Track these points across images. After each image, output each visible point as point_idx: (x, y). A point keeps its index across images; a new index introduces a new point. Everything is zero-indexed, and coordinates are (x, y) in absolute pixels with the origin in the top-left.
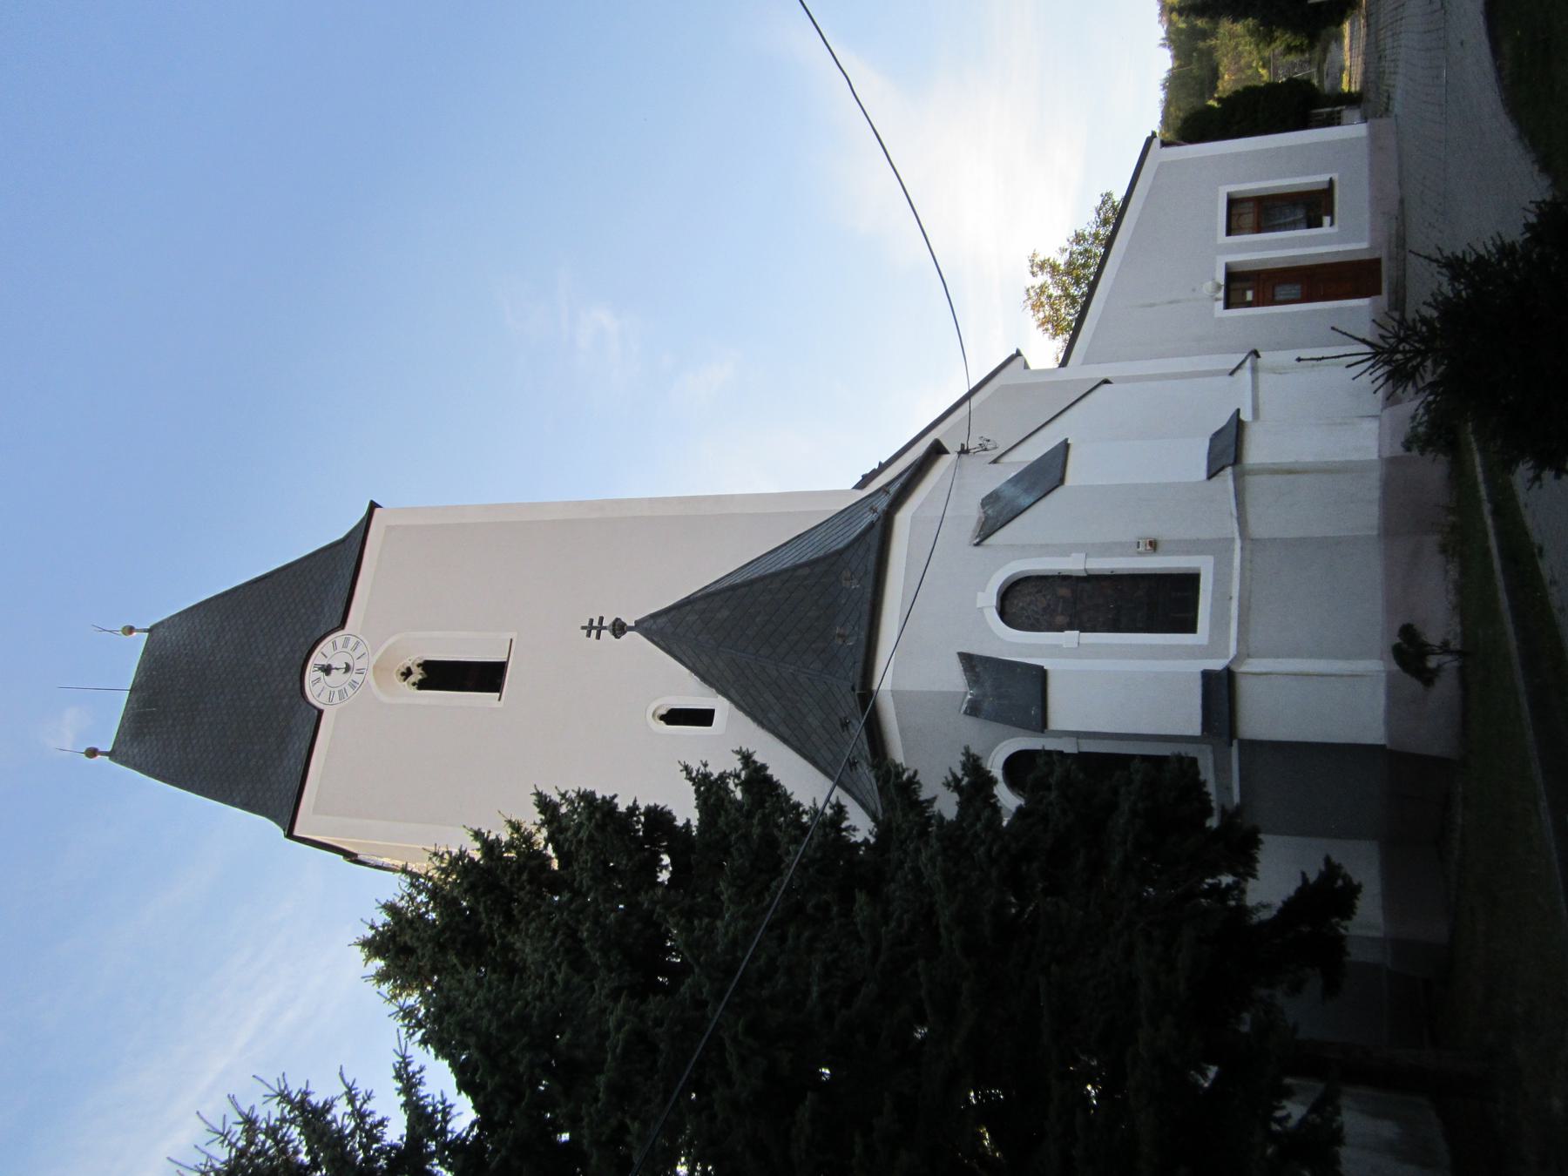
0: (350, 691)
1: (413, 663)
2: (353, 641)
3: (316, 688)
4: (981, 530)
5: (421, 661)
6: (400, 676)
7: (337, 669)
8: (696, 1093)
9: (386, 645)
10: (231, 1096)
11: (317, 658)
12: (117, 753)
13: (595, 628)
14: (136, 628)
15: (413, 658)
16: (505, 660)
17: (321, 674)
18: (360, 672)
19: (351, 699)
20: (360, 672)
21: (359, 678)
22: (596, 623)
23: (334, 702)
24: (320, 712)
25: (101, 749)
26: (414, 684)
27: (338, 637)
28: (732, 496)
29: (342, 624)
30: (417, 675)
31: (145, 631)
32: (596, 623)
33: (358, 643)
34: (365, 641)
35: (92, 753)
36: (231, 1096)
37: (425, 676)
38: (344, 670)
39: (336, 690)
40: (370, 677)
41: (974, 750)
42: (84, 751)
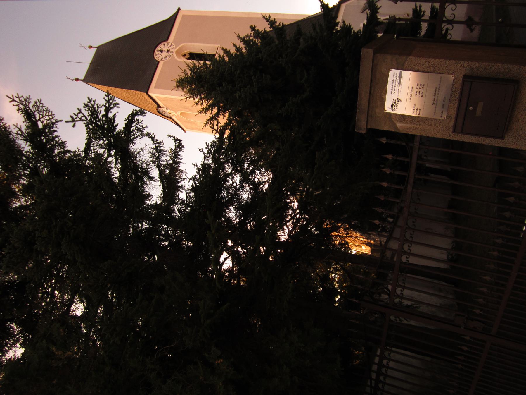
0: (168, 57)
1: (187, 53)
2: (170, 44)
3: (157, 56)
4: (364, 8)
5: (189, 52)
7: (165, 51)
8: (243, 217)
9: (180, 46)
11: (159, 48)
13: (249, 36)
14: (93, 46)
15: (187, 51)
16: (215, 54)
18: (172, 52)
20: (172, 52)
21: (171, 54)
22: (249, 35)
23: (163, 60)
24: (159, 62)
25: (80, 79)
26: (186, 58)
27: (166, 43)
28: (288, 14)
29: (167, 40)
30: (188, 56)
31: (96, 47)
32: (249, 35)
34: (174, 45)
35: (77, 80)
36: (154, 134)
39: (164, 57)
40: (175, 54)
41: (379, 13)
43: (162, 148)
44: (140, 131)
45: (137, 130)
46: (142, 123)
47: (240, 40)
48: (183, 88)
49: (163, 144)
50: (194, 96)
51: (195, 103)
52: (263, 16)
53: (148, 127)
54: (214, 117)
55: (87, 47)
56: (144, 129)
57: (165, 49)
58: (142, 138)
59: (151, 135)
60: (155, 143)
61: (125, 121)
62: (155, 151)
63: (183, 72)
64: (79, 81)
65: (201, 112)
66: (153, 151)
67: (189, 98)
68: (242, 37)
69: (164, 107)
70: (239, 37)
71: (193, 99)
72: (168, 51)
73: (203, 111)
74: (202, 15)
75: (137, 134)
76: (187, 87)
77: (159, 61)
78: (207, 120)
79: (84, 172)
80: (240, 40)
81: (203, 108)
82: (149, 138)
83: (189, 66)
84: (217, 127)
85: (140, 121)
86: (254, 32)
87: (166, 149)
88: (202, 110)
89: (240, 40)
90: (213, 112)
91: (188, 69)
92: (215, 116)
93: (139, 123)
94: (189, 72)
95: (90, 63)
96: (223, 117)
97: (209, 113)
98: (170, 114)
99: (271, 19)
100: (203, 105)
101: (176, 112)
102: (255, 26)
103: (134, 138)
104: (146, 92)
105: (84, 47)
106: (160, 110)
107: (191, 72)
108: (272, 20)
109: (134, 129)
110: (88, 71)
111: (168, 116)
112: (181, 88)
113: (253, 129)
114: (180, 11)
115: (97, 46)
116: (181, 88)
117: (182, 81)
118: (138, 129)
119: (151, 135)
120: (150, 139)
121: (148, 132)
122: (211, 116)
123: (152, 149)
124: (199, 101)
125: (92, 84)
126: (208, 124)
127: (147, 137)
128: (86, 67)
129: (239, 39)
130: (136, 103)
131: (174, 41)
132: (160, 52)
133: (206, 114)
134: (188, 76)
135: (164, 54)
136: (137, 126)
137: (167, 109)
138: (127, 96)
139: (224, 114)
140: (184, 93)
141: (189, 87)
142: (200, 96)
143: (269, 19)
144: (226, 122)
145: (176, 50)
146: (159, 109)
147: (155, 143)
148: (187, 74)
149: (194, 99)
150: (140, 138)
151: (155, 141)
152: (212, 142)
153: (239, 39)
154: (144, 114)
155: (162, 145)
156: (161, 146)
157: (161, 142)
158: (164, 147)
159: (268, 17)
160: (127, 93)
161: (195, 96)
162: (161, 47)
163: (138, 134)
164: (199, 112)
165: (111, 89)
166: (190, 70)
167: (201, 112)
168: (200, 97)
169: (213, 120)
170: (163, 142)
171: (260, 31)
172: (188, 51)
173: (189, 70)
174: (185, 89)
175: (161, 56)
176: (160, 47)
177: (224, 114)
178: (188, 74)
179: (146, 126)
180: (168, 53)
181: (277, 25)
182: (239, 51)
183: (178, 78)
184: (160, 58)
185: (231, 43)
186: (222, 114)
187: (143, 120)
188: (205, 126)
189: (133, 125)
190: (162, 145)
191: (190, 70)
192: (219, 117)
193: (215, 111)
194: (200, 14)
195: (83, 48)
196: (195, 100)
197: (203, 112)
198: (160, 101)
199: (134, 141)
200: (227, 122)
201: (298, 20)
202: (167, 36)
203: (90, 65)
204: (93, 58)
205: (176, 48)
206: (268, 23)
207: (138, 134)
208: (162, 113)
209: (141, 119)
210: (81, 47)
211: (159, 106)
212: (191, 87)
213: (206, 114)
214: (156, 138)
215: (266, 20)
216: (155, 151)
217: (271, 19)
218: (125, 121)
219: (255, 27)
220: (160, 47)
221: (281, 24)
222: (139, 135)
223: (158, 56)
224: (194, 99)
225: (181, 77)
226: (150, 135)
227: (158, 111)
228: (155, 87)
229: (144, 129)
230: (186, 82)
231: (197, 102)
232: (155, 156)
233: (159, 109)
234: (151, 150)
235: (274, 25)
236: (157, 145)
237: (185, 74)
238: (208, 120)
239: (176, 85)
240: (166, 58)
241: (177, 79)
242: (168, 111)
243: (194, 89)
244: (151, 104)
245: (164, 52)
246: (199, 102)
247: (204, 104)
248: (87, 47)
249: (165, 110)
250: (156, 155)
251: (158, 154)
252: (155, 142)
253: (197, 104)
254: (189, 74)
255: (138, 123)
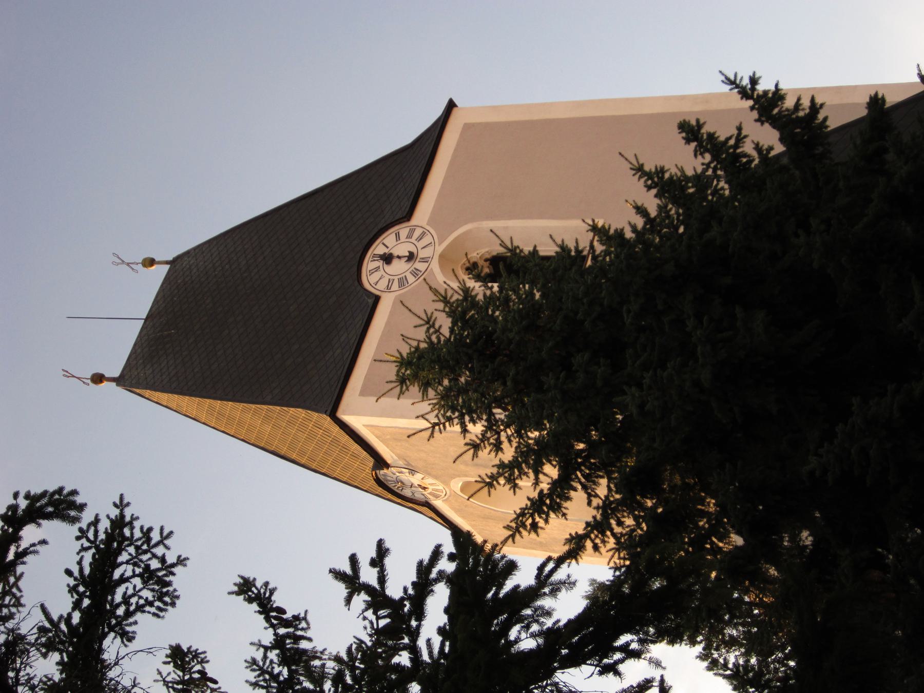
0: (411, 279)
1: (480, 257)
2: (418, 232)
5: (488, 256)
6: (464, 271)
7: (399, 257)
10: (270, 587)
11: (378, 248)
12: (126, 377)
14: (157, 259)
17: (380, 263)
18: (424, 260)
19: (412, 286)
20: (424, 260)
21: (422, 266)
24: (377, 299)
25: (107, 375)
27: (403, 230)
28: (855, 87)
31: (167, 263)
33: (423, 234)
34: (417, 282)
35: (98, 379)
36: (270, 587)
37: (493, 272)
38: (407, 258)
39: (396, 278)
40: (435, 266)
42: (141, 262)
43: (304, 645)
44: (157, 583)
45: (141, 575)
46: (168, 548)
47: (643, 180)
48: (425, 386)
49: (309, 628)
50: (462, 417)
51: (466, 444)
52: (727, 78)
53: (188, 562)
54: (548, 502)
55: (137, 264)
56: (173, 574)
57: (402, 250)
58: (161, 614)
59: (256, 591)
60: (275, 622)
61: (78, 538)
62: (276, 660)
63: (422, 322)
64: (105, 384)
65: (490, 483)
66: (265, 657)
67: (445, 427)
68: (653, 170)
69: (401, 463)
70: (639, 170)
71: (462, 427)
72: (411, 257)
73: (500, 475)
74: (536, 118)
75: (142, 594)
76: (440, 384)
77: (377, 293)
78: (518, 511)
79: (667, 564)
80: (645, 182)
81: (502, 465)
82: (250, 600)
83: (445, 298)
84: (376, 570)
85: (155, 536)
86: (695, 143)
87: (320, 648)
88: (498, 473)
89: (643, 180)
90: (541, 476)
91: (444, 311)
92: (550, 495)
93: (150, 548)
94: (445, 323)
95: (144, 317)
96: (586, 496)
97: (525, 483)
98: (424, 488)
99: (761, 88)
100: (501, 449)
101: (446, 483)
102: (702, 122)
103: (128, 614)
104: (328, 412)
105: (128, 264)
106: (385, 475)
107: (454, 323)
108: (766, 93)
109: (129, 573)
110: (135, 345)
111: (418, 496)
112: (415, 389)
113: (712, 543)
114: (455, 113)
115: (171, 258)
116: (415, 389)
117: (419, 358)
118: (148, 575)
119: (256, 591)
120: (255, 607)
121: (246, 576)
122: (535, 495)
123: (262, 650)
124: (483, 435)
125: (147, 393)
126: (524, 526)
127: (242, 597)
128: (131, 333)
129: (640, 178)
130: (302, 453)
131: (433, 220)
132: (382, 261)
133: (515, 487)
134: (442, 338)
135: (398, 267)
136: (145, 557)
137: (412, 471)
138: (268, 429)
139: (589, 484)
140: (425, 407)
141: (446, 382)
142: (491, 414)
143: (753, 89)
144: (590, 519)
145: (440, 249)
146: (382, 472)
147: (275, 622)
148: (437, 331)
149: (465, 431)
150: (154, 614)
151: (274, 614)
152: (345, 658)
153: (640, 178)
154: (73, 513)
155: (302, 629)
156: (299, 633)
157: (296, 618)
158: (310, 639)
159: (746, 82)
160: (267, 419)
161: (467, 418)
162: (388, 242)
163: (147, 594)
164: (484, 482)
165: (210, 406)
166: (447, 313)
167: (490, 483)
168: (488, 420)
169: (544, 512)
170: (305, 619)
171: (722, 138)
172: (487, 250)
173: (444, 315)
174: (431, 393)
175: (387, 277)
176: (384, 244)
177: (589, 484)
178: (441, 331)
179: (179, 557)
180: (410, 264)
181: (787, 110)
182: (660, 231)
183: (405, 351)
184: (382, 285)
185: (627, 201)
186: (579, 487)
187: (171, 533)
188: (513, 536)
189: (124, 557)
190: (302, 629)
191: (449, 315)
192: (568, 499)
193: (551, 471)
194: (527, 117)
195: (125, 266)
196: (467, 435)
197: (502, 481)
198: (384, 441)
199: (128, 629)
200: (594, 517)
201: (893, 104)
202: (408, 204)
203: (145, 323)
204: (156, 301)
205: (440, 244)
206: (750, 103)
207: (147, 594)
208: (395, 489)
209: (162, 529)
210: (118, 264)
211: (380, 462)
212: (454, 380)
213: (515, 487)
214: (278, 600)
215: (739, 93)
216: (273, 655)
217: (761, 88)
218: (78, 538)
219: (700, 126)
220: (384, 244)
221: (806, 103)
222: (151, 598)
223: (374, 278)
224: (465, 431)
225: (415, 344)
226: (254, 589)
227: (380, 482)
228: (364, 392)
229: (173, 574)
230: (433, 361)
231: (478, 442)
232: (275, 677)
233: (382, 472)
234: (259, 655)
235: (776, 111)
236: (282, 631)
237: (428, 329)
238: (522, 514)
239: (397, 375)
240: (402, 282)
241: (400, 354)
242: (416, 479)
243: (463, 391)
244: (355, 456)
245: (395, 262)
246: (484, 438)
247: (505, 445)
248: (137, 264)
249: (406, 477)
250: (280, 674)
251: (290, 671)
252: (275, 618)
253: (476, 447)
254: (446, 331)
255: (145, 547)
